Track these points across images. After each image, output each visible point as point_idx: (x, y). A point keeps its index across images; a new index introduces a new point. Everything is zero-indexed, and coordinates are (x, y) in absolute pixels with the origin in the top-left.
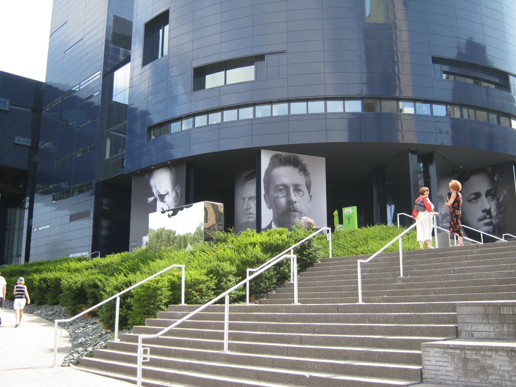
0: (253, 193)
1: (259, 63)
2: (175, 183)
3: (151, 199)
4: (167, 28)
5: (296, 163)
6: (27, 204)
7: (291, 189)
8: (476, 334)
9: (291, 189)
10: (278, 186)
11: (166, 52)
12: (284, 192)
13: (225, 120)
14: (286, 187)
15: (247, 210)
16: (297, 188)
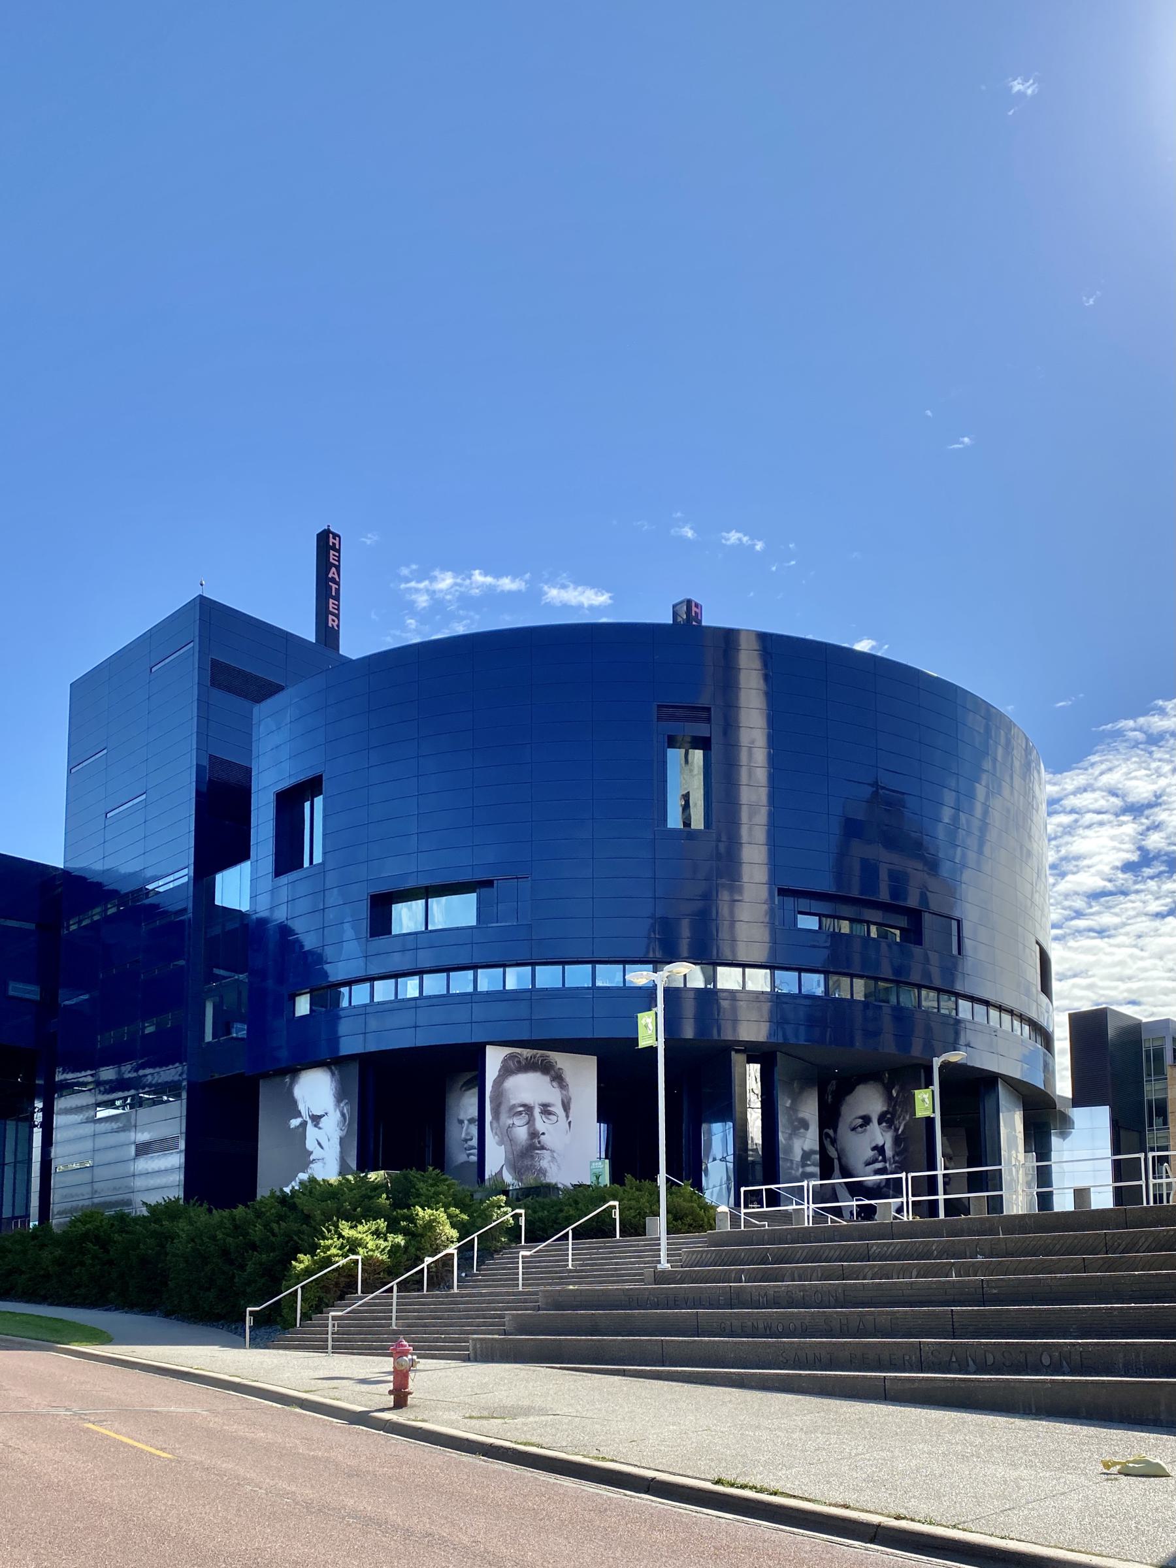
0: (474, 1112)
1: (484, 890)
2: (341, 1096)
3: (295, 1123)
4: (319, 801)
5: (545, 1068)
6: (38, 1117)
7: (537, 1111)
10: (514, 1106)
11: (318, 859)
12: (524, 1118)
13: (421, 902)
14: (528, 1109)
15: (466, 1141)
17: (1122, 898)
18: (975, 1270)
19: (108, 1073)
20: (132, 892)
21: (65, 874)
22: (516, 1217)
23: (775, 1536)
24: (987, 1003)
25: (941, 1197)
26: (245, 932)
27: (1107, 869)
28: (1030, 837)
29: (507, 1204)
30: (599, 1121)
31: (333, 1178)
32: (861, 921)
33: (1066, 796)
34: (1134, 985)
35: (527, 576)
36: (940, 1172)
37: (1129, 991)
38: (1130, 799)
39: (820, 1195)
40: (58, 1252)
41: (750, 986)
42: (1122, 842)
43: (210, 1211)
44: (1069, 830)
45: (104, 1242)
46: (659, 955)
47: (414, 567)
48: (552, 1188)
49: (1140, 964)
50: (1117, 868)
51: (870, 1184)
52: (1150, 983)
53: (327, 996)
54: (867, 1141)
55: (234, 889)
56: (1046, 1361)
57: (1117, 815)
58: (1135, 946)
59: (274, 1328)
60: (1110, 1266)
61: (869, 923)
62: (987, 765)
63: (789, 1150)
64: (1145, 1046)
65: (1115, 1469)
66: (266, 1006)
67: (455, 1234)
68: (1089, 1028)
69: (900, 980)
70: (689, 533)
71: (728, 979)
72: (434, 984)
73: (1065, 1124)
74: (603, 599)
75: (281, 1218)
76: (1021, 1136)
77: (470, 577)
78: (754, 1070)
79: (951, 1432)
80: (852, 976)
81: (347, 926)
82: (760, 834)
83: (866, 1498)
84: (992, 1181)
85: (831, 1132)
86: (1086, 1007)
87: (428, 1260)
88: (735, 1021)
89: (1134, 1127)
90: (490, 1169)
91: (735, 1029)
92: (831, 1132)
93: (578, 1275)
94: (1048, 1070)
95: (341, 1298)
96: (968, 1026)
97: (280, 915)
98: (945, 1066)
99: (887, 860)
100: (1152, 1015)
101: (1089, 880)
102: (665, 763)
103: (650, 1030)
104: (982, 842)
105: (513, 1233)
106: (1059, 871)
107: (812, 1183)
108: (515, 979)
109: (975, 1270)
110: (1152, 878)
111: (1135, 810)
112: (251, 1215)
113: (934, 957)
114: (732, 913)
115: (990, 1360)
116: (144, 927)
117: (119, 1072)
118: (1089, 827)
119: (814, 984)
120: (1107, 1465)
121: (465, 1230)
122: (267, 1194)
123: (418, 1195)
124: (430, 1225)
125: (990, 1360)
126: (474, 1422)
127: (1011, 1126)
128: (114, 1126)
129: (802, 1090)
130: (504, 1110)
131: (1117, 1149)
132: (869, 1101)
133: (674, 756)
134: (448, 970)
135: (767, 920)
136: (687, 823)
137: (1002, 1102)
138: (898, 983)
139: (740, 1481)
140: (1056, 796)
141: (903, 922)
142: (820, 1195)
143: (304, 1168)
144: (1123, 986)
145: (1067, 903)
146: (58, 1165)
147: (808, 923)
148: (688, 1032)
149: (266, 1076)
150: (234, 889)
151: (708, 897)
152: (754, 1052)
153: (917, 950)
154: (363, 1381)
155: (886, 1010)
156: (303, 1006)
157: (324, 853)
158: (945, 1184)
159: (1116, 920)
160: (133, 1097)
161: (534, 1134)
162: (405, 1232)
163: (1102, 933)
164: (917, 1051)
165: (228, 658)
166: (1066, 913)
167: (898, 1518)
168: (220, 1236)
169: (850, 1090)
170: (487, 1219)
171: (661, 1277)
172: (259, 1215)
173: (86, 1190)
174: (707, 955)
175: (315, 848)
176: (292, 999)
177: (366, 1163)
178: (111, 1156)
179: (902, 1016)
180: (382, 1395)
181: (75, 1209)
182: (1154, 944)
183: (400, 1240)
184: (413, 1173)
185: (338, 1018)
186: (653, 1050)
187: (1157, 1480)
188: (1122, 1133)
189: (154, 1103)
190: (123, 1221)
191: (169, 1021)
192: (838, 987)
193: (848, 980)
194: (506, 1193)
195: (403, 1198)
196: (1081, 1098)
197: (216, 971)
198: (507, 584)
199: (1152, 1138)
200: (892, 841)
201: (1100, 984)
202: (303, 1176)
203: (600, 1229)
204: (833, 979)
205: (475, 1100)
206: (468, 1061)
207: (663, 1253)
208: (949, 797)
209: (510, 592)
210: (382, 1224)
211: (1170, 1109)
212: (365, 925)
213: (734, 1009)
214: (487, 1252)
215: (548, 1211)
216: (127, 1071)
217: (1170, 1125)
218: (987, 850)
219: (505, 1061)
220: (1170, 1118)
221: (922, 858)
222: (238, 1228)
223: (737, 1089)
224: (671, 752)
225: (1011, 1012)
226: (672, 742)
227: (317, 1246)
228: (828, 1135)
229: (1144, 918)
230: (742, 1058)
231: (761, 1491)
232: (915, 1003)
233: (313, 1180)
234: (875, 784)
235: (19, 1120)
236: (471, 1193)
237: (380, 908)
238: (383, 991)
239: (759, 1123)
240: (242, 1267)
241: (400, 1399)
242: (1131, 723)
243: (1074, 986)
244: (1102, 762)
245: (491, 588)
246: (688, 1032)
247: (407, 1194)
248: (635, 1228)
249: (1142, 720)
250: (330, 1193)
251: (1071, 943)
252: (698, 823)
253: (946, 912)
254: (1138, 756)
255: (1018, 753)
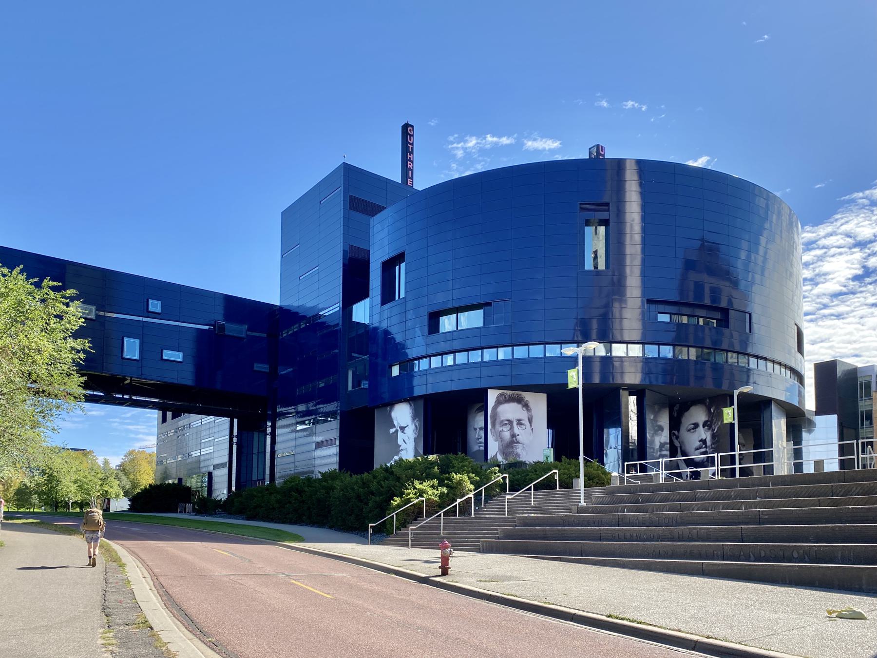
2: (415, 417)
3: (392, 430)
4: (403, 265)
5: (519, 400)
6: (269, 430)
7: (515, 423)
8: (260, 477)
9: (515, 423)
10: (502, 421)
11: (402, 295)
12: (508, 427)
13: (455, 315)
14: (510, 422)
16: (520, 423)
17: (851, 296)
18: (756, 505)
19: (302, 408)
20: (313, 316)
21: (281, 308)
22: (504, 478)
23: (639, 645)
24: (766, 359)
25: (737, 466)
26: (368, 336)
27: (843, 280)
28: (792, 265)
29: (499, 472)
30: (548, 428)
31: (411, 458)
32: (694, 316)
33: (820, 239)
34: (857, 346)
35: (516, 135)
36: (737, 453)
37: (855, 349)
38: (859, 239)
39: (668, 467)
40: (279, 497)
41: (631, 354)
42: (853, 264)
43: (351, 475)
44: (821, 258)
45: (300, 492)
46: (580, 339)
47: (456, 135)
48: (523, 464)
49: (862, 333)
50: (849, 279)
51: (698, 460)
52: (867, 344)
53: (407, 365)
54: (696, 438)
55: (362, 313)
56: (795, 555)
57: (850, 248)
58: (859, 323)
59: (382, 535)
60: (835, 503)
61: (698, 317)
62: (767, 226)
63: (653, 442)
64: (859, 380)
65: (834, 615)
66: (377, 372)
67: (472, 487)
68: (826, 372)
69: (716, 348)
70: (605, 104)
71: (619, 350)
72: (461, 358)
73: (811, 425)
74: (556, 145)
75: (386, 479)
76: (784, 432)
77: (485, 138)
78: (633, 399)
79: (740, 593)
80: (688, 346)
81: (417, 329)
82: (637, 271)
83: (691, 627)
84: (769, 456)
85: (676, 433)
86: (827, 359)
87: (459, 500)
88: (622, 373)
89: (852, 425)
90: (491, 454)
91: (622, 377)
92: (676, 433)
93: (536, 509)
94: (801, 396)
95: (416, 520)
96: (755, 372)
97: (384, 325)
98: (741, 395)
99: (709, 282)
100: (868, 362)
101: (832, 287)
102: (584, 234)
103: (575, 379)
104: (763, 269)
105: (503, 487)
106: (814, 281)
107: (665, 459)
108: (503, 354)
109: (756, 505)
110: (870, 284)
111: (861, 245)
112: (371, 477)
113: (736, 335)
114: (621, 315)
115: (763, 554)
116: (319, 334)
117: (307, 407)
118: (833, 256)
119: (667, 352)
120: (829, 612)
121: (477, 485)
122: (378, 467)
123: (454, 467)
124: (460, 483)
125: (763, 554)
126: (482, 583)
127: (779, 426)
128: (305, 433)
129: (660, 410)
130: (498, 422)
131: (841, 437)
132: (698, 415)
133: (589, 230)
134: (468, 350)
135: (640, 317)
136: (596, 267)
137: (774, 414)
138: (715, 349)
139: (621, 616)
140: (814, 239)
141: (718, 315)
142: (668, 467)
143: (397, 454)
144: (850, 346)
145: (818, 300)
146: (278, 454)
147: (664, 318)
148: (596, 379)
149: (378, 407)
150: (362, 313)
151: (608, 306)
152: (633, 390)
153: (726, 331)
154: (426, 562)
155: (708, 364)
156: (396, 371)
157: (406, 292)
158: (740, 460)
159: (848, 309)
160: (314, 419)
161: (513, 436)
162: (447, 486)
163: (839, 316)
164: (725, 387)
165: (359, 193)
166: (818, 306)
167: (609, 616)
168: (356, 487)
169: (687, 409)
170: (489, 479)
171: (581, 510)
172: (375, 477)
173: (292, 466)
174: (606, 338)
175: (401, 290)
176: (390, 367)
177: (427, 451)
178: (304, 448)
179: (717, 368)
180: (434, 570)
181: (287, 476)
182: (870, 322)
183: (445, 490)
184: (451, 456)
185: (413, 376)
186: (576, 390)
187: (859, 621)
188: (845, 430)
189: (324, 422)
190: (309, 481)
191: (331, 380)
192: (681, 352)
193: (686, 349)
194: (499, 466)
195: (446, 469)
196: (822, 409)
197: (353, 354)
198: (505, 141)
199: (863, 432)
200: (712, 272)
201: (837, 345)
202: (396, 458)
203: (549, 485)
204: (678, 348)
205: (482, 418)
206: (480, 396)
207: (582, 498)
208: (745, 245)
209: (507, 146)
210: (435, 482)
211: (874, 416)
212: (426, 329)
213: (622, 366)
214: (489, 497)
215: (521, 475)
216: (311, 406)
217: (874, 425)
218: (766, 273)
219: (498, 397)
220: (874, 421)
221: (729, 280)
222: (365, 484)
223: (623, 410)
224: (587, 229)
225: (780, 364)
226: (588, 223)
227: (404, 493)
228: (674, 434)
229: (865, 307)
230: (627, 393)
231: (633, 621)
232: (724, 360)
233: (401, 459)
234: (702, 240)
235: (259, 432)
236: (481, 467)
237: (434, 319)
238: (435, 362)
239: (635, 428)
240: (367, 504)
241: (445, 572)
242: (861, 194)
243: (821, 347)
244: (842, 218)
245: (496, 144)
246: (596, 379)
247: (448, 466)
248: (567, 484)
249: (867, 192)
250: (410, 466)
251: (820, 323)
252: (602, 266)
253: (741, 309)
254: (864, 213)
255: (785, 218)
